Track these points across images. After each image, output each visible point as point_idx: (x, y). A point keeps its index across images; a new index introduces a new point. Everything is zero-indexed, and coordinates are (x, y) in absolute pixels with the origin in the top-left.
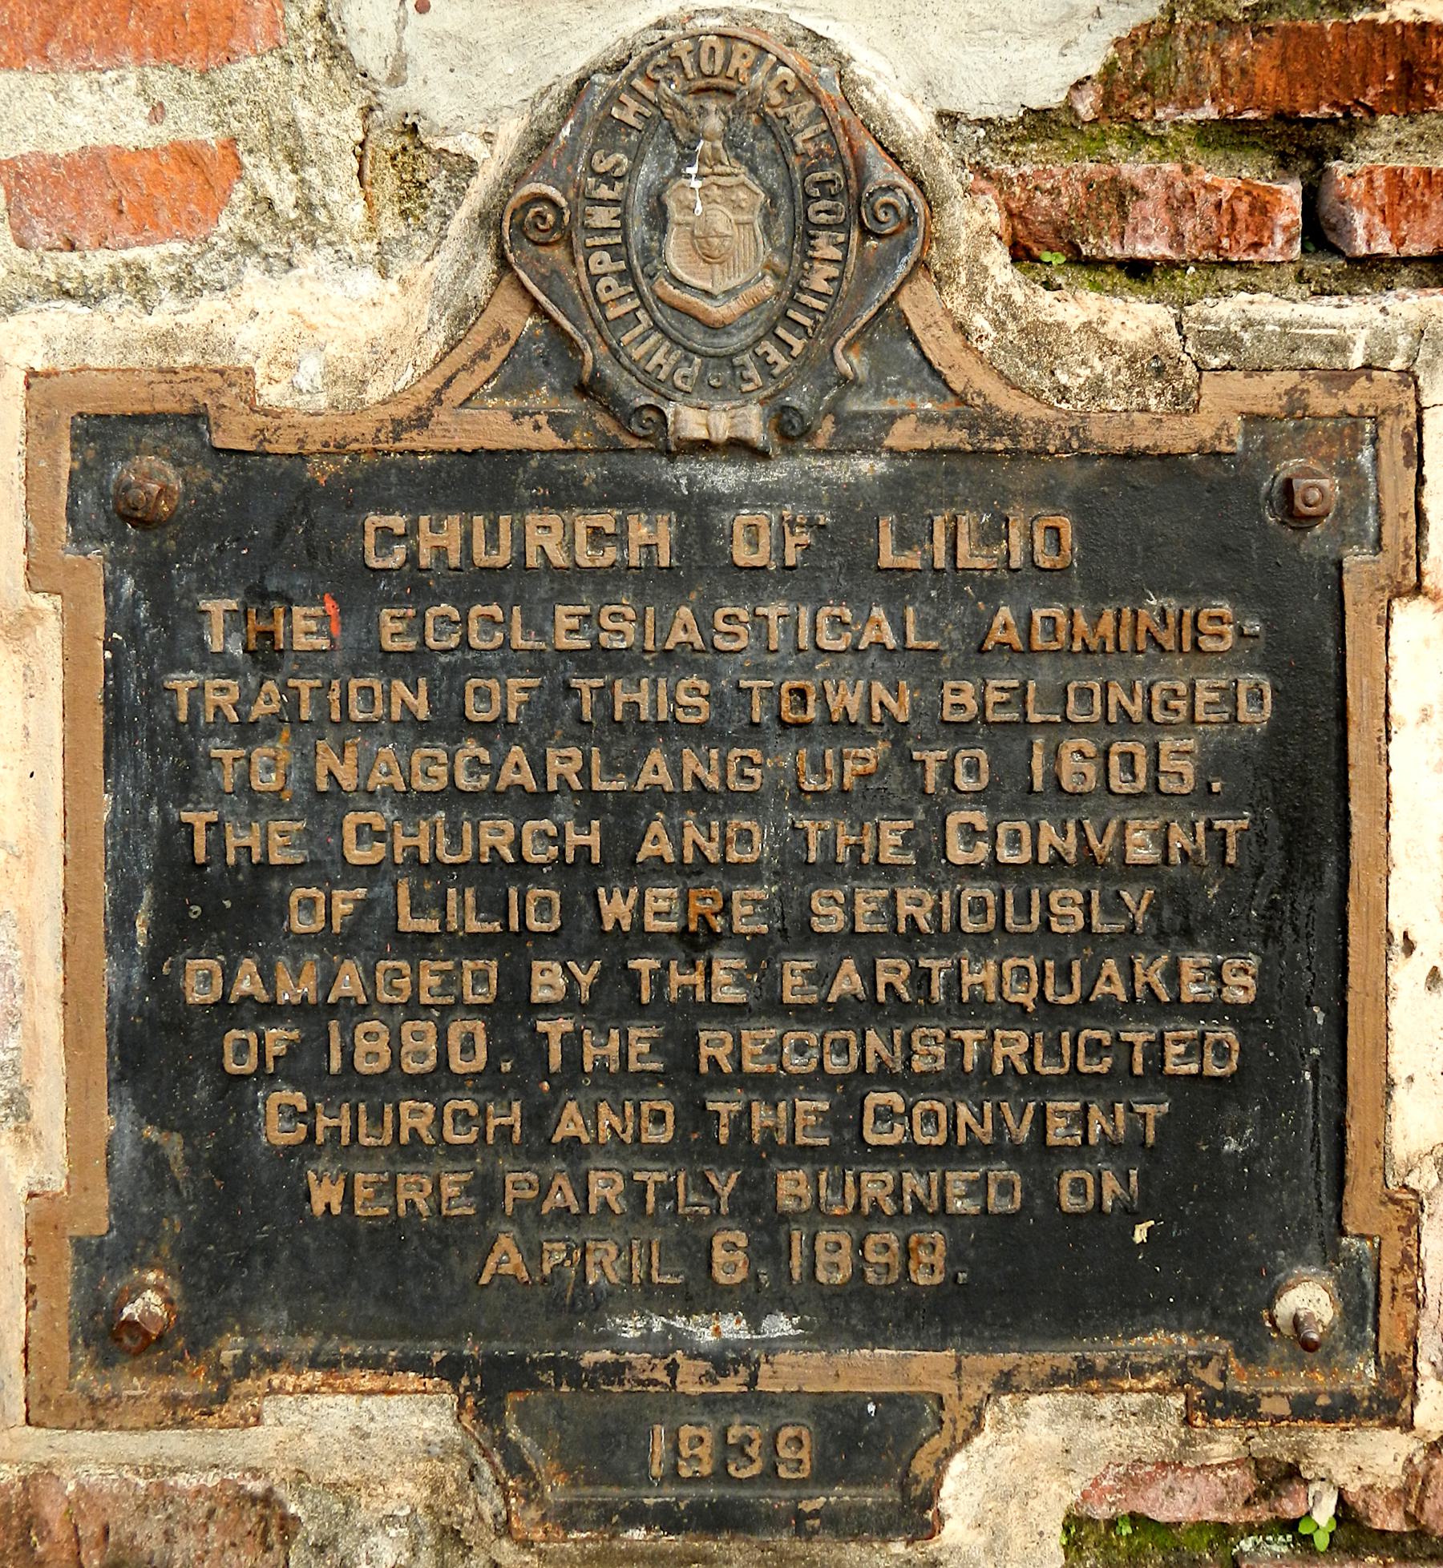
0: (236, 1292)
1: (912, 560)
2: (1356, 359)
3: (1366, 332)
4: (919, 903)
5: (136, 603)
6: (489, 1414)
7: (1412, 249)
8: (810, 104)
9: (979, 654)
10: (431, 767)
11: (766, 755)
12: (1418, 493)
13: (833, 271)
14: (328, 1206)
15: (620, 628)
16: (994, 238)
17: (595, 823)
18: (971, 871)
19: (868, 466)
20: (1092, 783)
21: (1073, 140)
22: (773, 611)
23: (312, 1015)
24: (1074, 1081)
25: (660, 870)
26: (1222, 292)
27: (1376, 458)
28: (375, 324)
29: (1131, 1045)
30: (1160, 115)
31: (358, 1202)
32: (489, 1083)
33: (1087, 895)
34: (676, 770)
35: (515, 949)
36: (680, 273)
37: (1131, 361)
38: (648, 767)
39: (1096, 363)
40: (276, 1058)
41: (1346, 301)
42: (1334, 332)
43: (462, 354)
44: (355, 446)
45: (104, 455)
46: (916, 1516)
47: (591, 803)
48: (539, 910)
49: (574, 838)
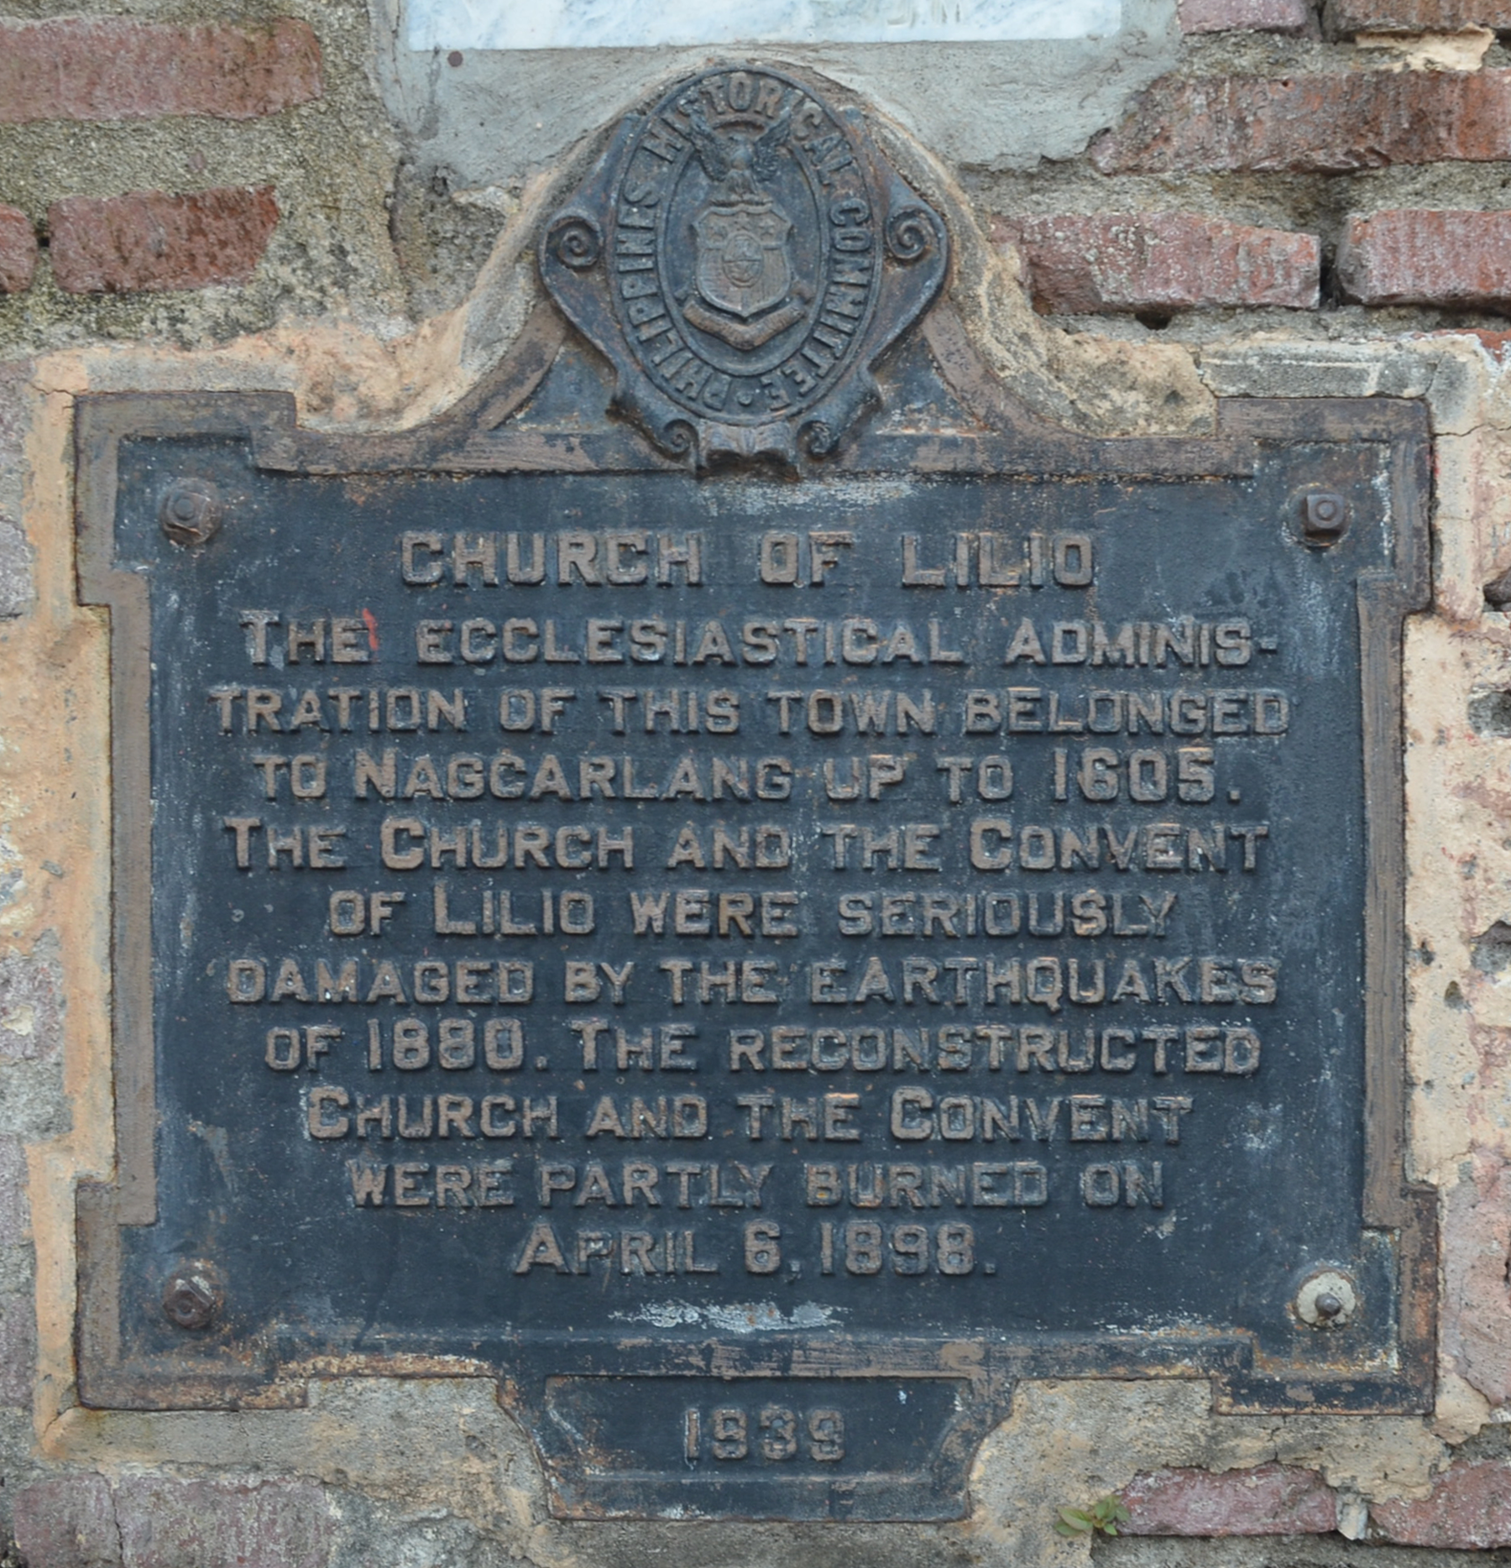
1: (934, 576)
2: (1370, 388)
5: (180, 615)
6: (530, 1398)
10: (466, 774)
11: (794, 765)
13: (858, 294)
14: (369, 1194)
15: (653, 637)
17: (628, 829)
22: (799, 624)
24: (1094, 1077)
25: (689, 871)
31: (399, 1191)
34: (706, 776)
35: (546, 947)
38: (680, 774)
46: (945, 1491)
48: (570, 909)
49: (606, 843)
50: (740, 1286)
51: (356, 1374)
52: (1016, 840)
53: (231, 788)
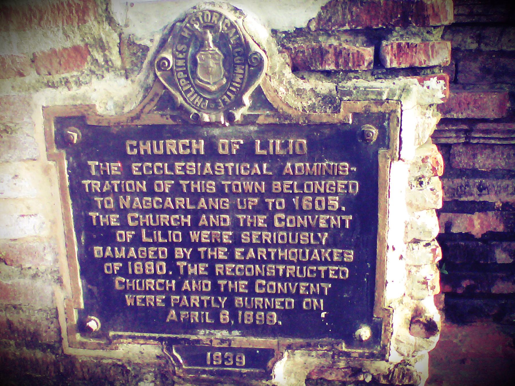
0: (111, 322)
1: (265, 152)
2: (384, 97)
3: (388, 90)
4: (268, 236)
7: (403, 66)
8: (234, 30)
9: (281, 176)
12: (400, 133)
13: (242, 76)
16: (287, 65)
18: (281, 229)
19: (252, 128)
20: (311, 208)
21: (309, 37)
22: (230, 165)
23: (124, 261)
24: (307, 279)
26: (350, 79)
27: (389, 124)
28: (125, 92)
29: (320, 271)
30: (333, 29)
32: (166, 276)
33: (309, 235)
35: (171, 246)
36: (201, 78)
37: (323, 99)
39: (313, 99)
40: (117, 270)
41: (384, 81)
42: (379, 90)
43: (147, 100)
44: (122, 124)
45: (62, 127)
46: (268, 375)
47: (186, 212)
48: (176, 236)
50: (217, 325)
51: (129, 343)
52: (285, 220)
53: (91, 206)
